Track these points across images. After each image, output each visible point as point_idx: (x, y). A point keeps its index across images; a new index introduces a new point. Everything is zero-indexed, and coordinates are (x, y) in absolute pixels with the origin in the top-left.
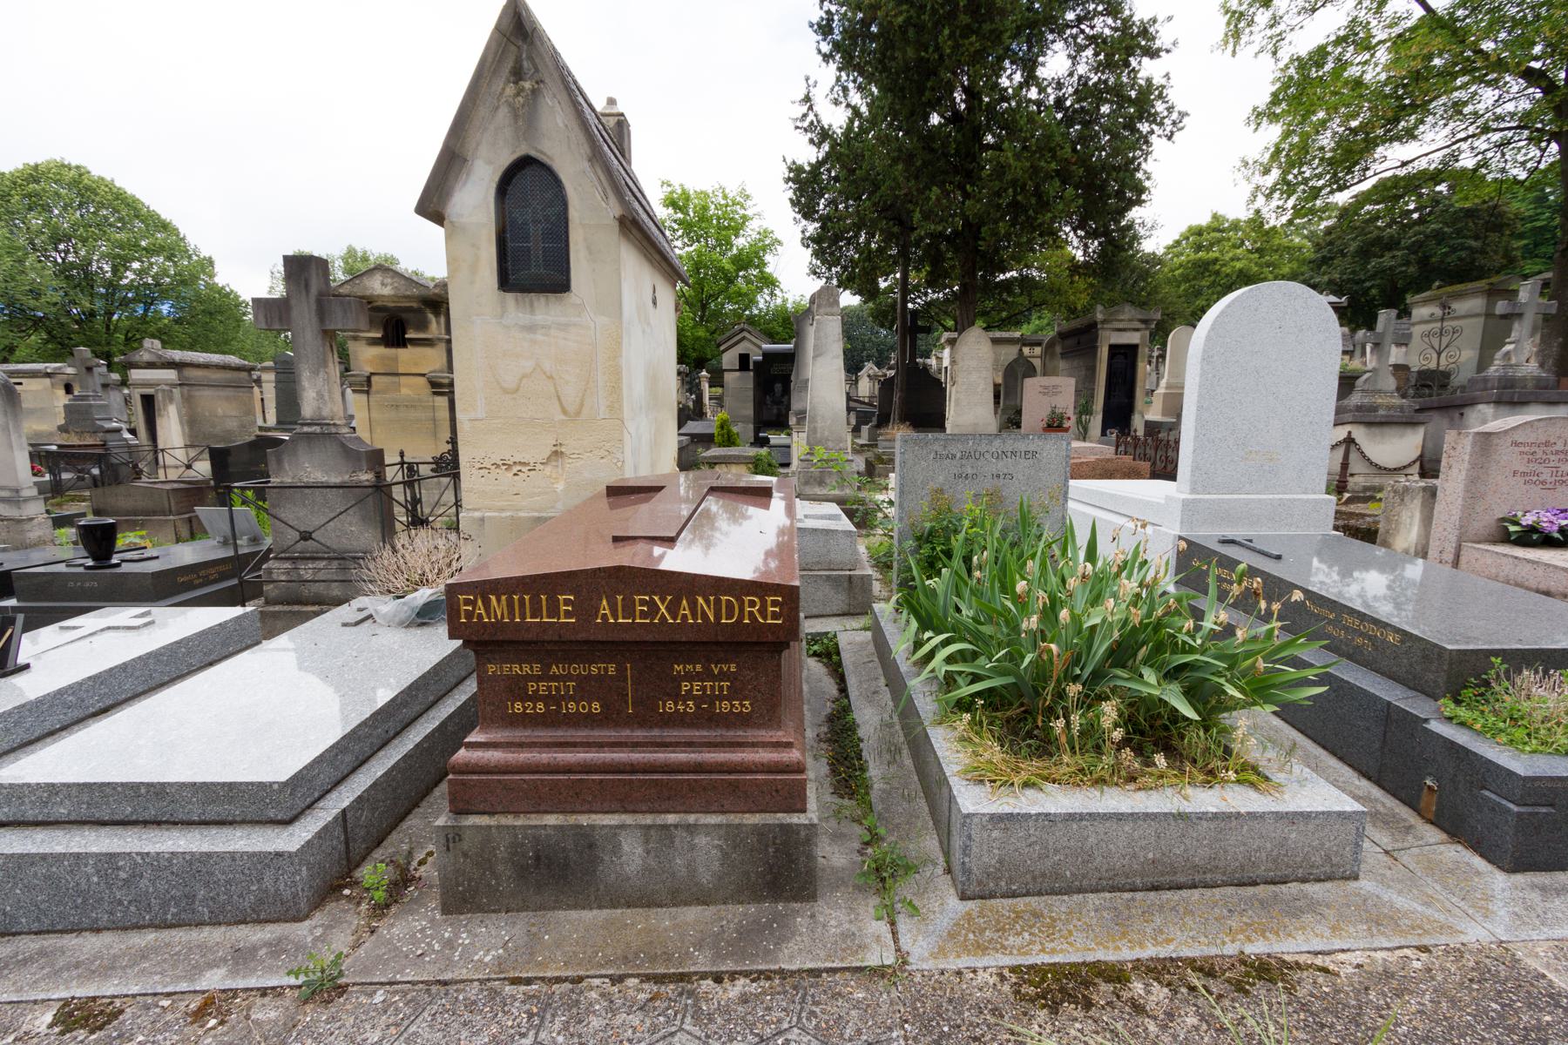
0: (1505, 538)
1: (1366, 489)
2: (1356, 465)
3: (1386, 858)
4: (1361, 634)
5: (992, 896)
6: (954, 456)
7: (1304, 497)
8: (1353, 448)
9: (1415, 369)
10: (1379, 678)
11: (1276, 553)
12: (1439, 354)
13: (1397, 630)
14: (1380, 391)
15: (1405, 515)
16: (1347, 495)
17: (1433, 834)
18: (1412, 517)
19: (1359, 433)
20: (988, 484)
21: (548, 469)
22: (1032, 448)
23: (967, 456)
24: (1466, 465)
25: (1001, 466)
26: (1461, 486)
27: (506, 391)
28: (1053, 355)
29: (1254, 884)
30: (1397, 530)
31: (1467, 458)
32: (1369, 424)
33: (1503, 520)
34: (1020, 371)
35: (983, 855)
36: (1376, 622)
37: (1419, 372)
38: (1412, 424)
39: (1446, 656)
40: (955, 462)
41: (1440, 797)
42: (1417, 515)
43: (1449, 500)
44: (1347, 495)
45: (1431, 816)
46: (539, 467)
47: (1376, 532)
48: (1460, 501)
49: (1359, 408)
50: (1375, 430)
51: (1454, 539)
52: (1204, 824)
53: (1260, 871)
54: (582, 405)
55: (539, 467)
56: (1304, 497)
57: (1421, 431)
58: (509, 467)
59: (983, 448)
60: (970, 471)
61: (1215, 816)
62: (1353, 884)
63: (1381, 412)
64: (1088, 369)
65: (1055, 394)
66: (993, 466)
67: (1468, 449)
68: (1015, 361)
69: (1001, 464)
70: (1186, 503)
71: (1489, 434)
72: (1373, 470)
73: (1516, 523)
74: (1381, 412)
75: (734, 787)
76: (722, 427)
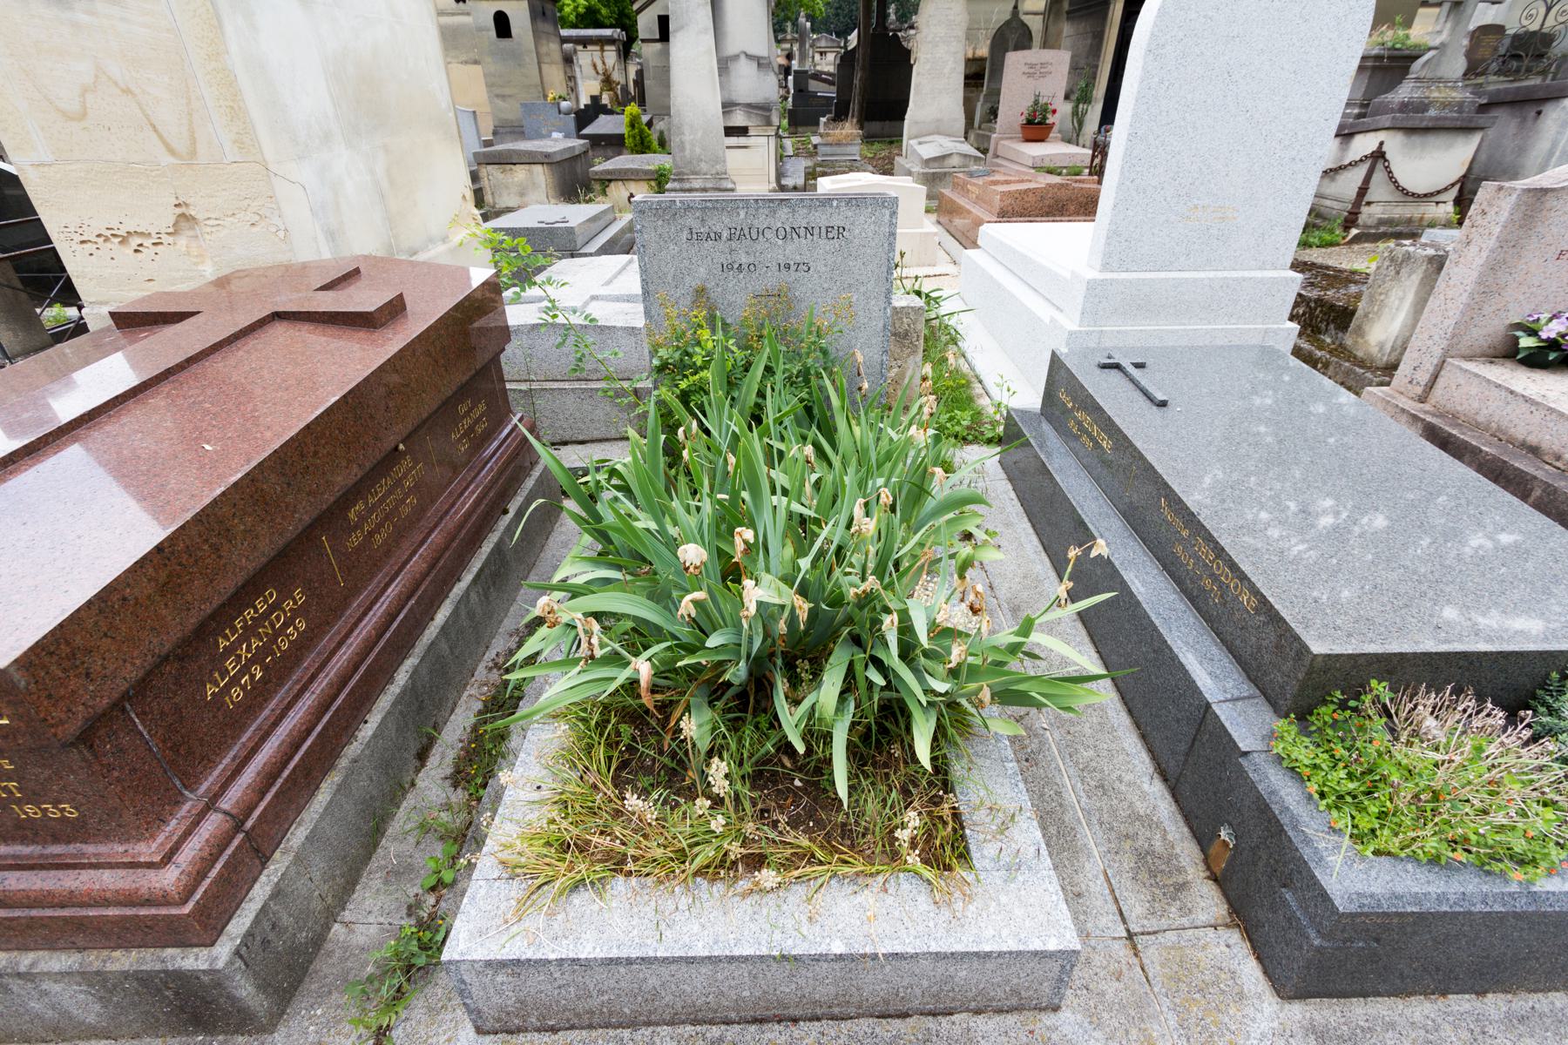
0: (1508, 352)
1: (1381, 222)
2: (1379, 190)
3: (1121, 950)
4: (1215, 578)
5: (519, 1030)
6: (718, 236)
7: (1258, 274)
8: (1380, 166)
9: (1510, 32)
10: (1217, 651)
11: (1160, 397)
12: (1549, 9)
13: (1256, 592)
14: (1440, 80)
15: (1393, 299)
16: (1354, 231)
17: (1208, 902)
18: (1402, 299)
19: (1394, 144)
20: (771, 280)
21: (182, 241)
22: (837, 221)
23: (737, 235)
24: (1492, 243)
25: (792, 250)
26: (1475, 274)
27: (68, 117)
28: (1058, 14)
29: (904, 1015)
30: (1378, 314)
31: (1497, 230)
32: (1410, 131)
33: (1519, 326)
34: (1013, 38)
35: (498, 995)
36: (1233, 566)
37: (1516, 37)
38: (1466, 129)
39: (1307, 662)
40: (721, 245)
41: (1233, 858)
42: (1410, 297)
43: (1450, 293)
44: (1354, 231)
45: (1217, 871)
46: (166, 239)
47: (1353, 313)
48: (1464, 298)
49: (1404, 107)
50: (1417, 139)
51: (1437, 352)
52: (825, 965)
53: (916, 1004)
54: (193, 141)
55: (166, 239)
56: (1258, 274)
57: (1476, 139)
58: (124, 241)
59: (761, 222)
60: (744, 260)
61: (840, 958)
62: (1048, 1019)
63: (1432, 113)
64: (1094, 37)
65: (1043, 75)
66: (776, 251)
67: (1504, 216)
68: (1007, 23)
69: (790, 247)
70: (1092, 286)
71: (1545, 191)
72: (1398, 196)
73: (1533, 333)
74: (1432, 113)
75: (80, 925)
76: (632, 126)
